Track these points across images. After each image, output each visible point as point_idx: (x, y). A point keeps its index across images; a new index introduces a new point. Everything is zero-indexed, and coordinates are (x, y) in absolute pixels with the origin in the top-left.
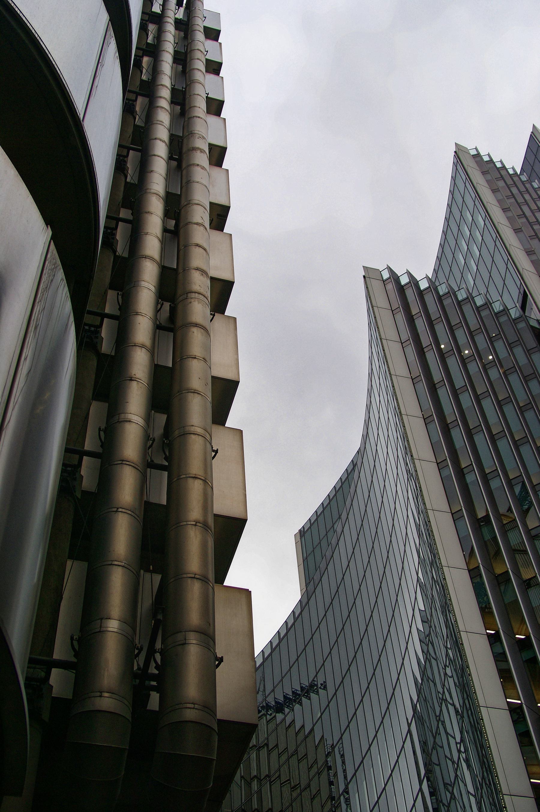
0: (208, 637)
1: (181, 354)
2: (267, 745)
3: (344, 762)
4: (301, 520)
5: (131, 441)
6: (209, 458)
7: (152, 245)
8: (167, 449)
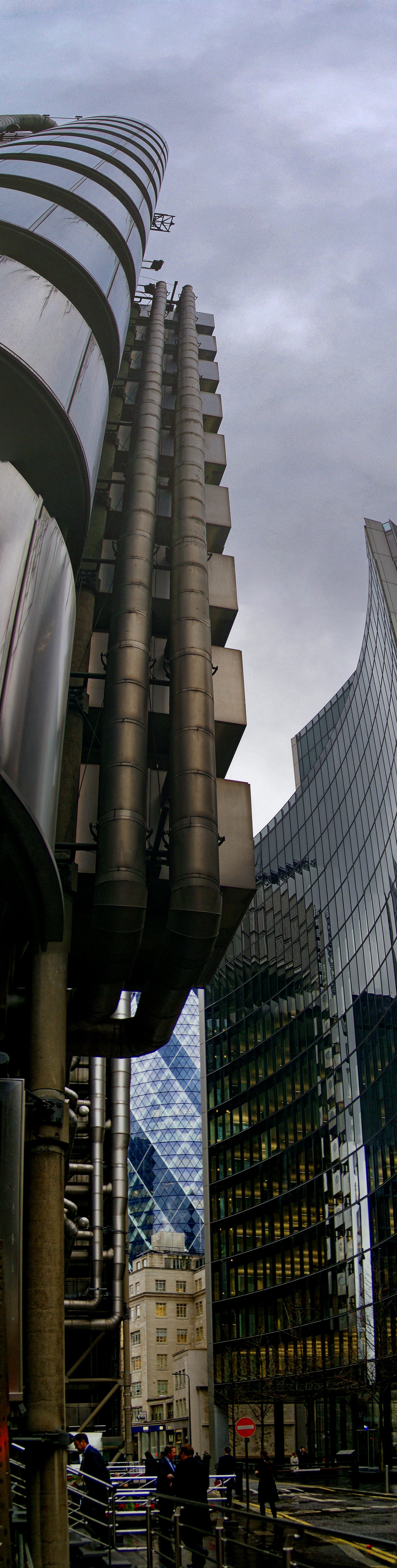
0: (210, 820)
1: (178, 589)
2: (264, 908)
3: (329, 924)
4: (298, 727)
5: (133, 662)
6: (209, 675)
7: (146, 499)
8: (168, 666)
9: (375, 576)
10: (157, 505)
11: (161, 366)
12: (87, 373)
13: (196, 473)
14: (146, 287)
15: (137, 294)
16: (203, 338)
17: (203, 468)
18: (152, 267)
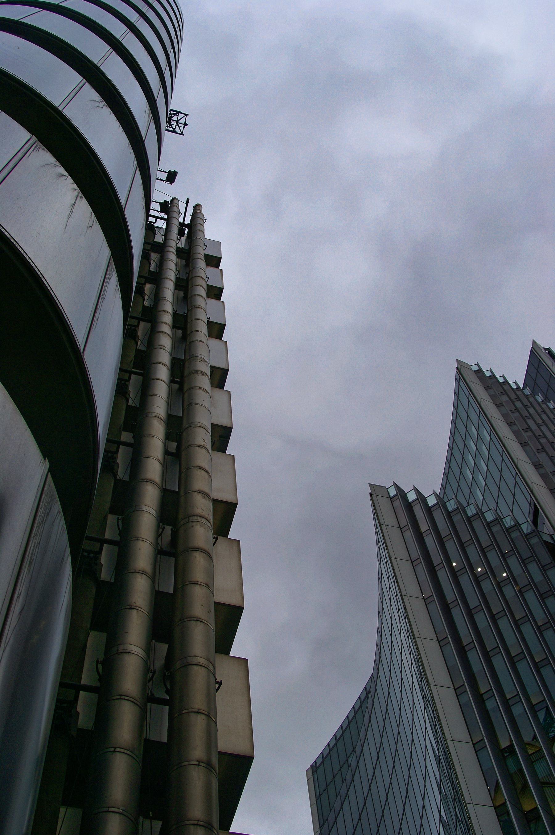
1: (182, 580)
5: (130, 676)
7: (153, 468)
8: (168, 682)
9: (384, 554)
10: (164, 475)
11: (172, 304)
12: (105, 305)
13: (203, 437)
14: (161, 204)
15: (151, 213)
16: (211, 271)
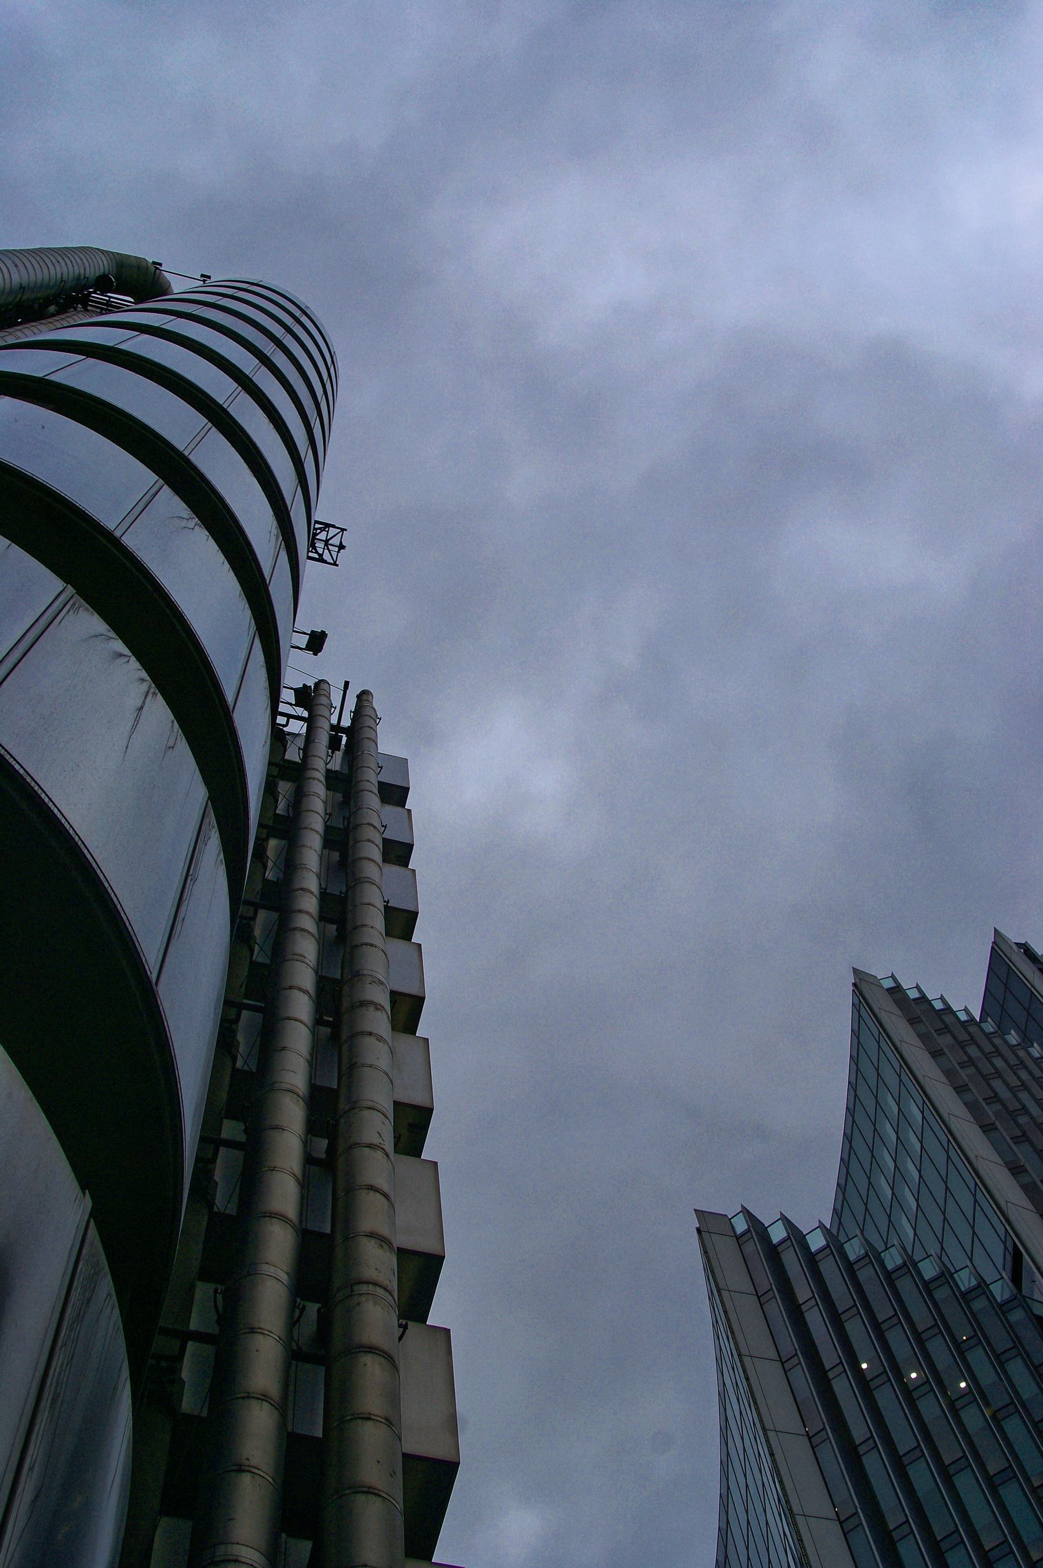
7: (284, 1192)
10: (305, 1202)
11: (319, 877)
13: (377, 1128)
14: (297, 691)
15: (282, 708)
17: (391, 1115)
18: (309, 647)
